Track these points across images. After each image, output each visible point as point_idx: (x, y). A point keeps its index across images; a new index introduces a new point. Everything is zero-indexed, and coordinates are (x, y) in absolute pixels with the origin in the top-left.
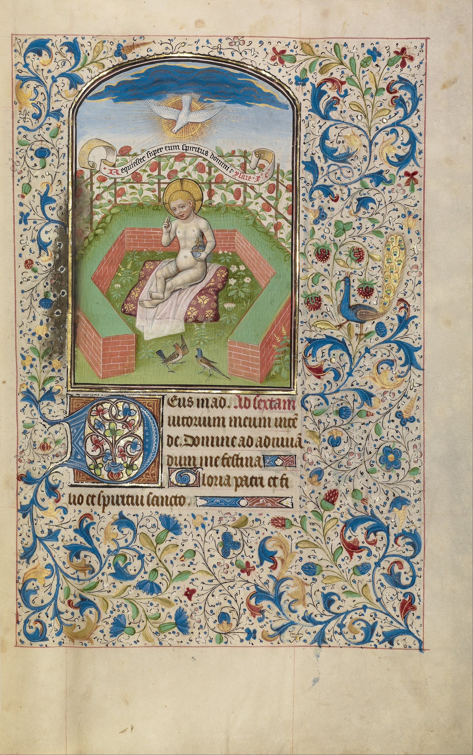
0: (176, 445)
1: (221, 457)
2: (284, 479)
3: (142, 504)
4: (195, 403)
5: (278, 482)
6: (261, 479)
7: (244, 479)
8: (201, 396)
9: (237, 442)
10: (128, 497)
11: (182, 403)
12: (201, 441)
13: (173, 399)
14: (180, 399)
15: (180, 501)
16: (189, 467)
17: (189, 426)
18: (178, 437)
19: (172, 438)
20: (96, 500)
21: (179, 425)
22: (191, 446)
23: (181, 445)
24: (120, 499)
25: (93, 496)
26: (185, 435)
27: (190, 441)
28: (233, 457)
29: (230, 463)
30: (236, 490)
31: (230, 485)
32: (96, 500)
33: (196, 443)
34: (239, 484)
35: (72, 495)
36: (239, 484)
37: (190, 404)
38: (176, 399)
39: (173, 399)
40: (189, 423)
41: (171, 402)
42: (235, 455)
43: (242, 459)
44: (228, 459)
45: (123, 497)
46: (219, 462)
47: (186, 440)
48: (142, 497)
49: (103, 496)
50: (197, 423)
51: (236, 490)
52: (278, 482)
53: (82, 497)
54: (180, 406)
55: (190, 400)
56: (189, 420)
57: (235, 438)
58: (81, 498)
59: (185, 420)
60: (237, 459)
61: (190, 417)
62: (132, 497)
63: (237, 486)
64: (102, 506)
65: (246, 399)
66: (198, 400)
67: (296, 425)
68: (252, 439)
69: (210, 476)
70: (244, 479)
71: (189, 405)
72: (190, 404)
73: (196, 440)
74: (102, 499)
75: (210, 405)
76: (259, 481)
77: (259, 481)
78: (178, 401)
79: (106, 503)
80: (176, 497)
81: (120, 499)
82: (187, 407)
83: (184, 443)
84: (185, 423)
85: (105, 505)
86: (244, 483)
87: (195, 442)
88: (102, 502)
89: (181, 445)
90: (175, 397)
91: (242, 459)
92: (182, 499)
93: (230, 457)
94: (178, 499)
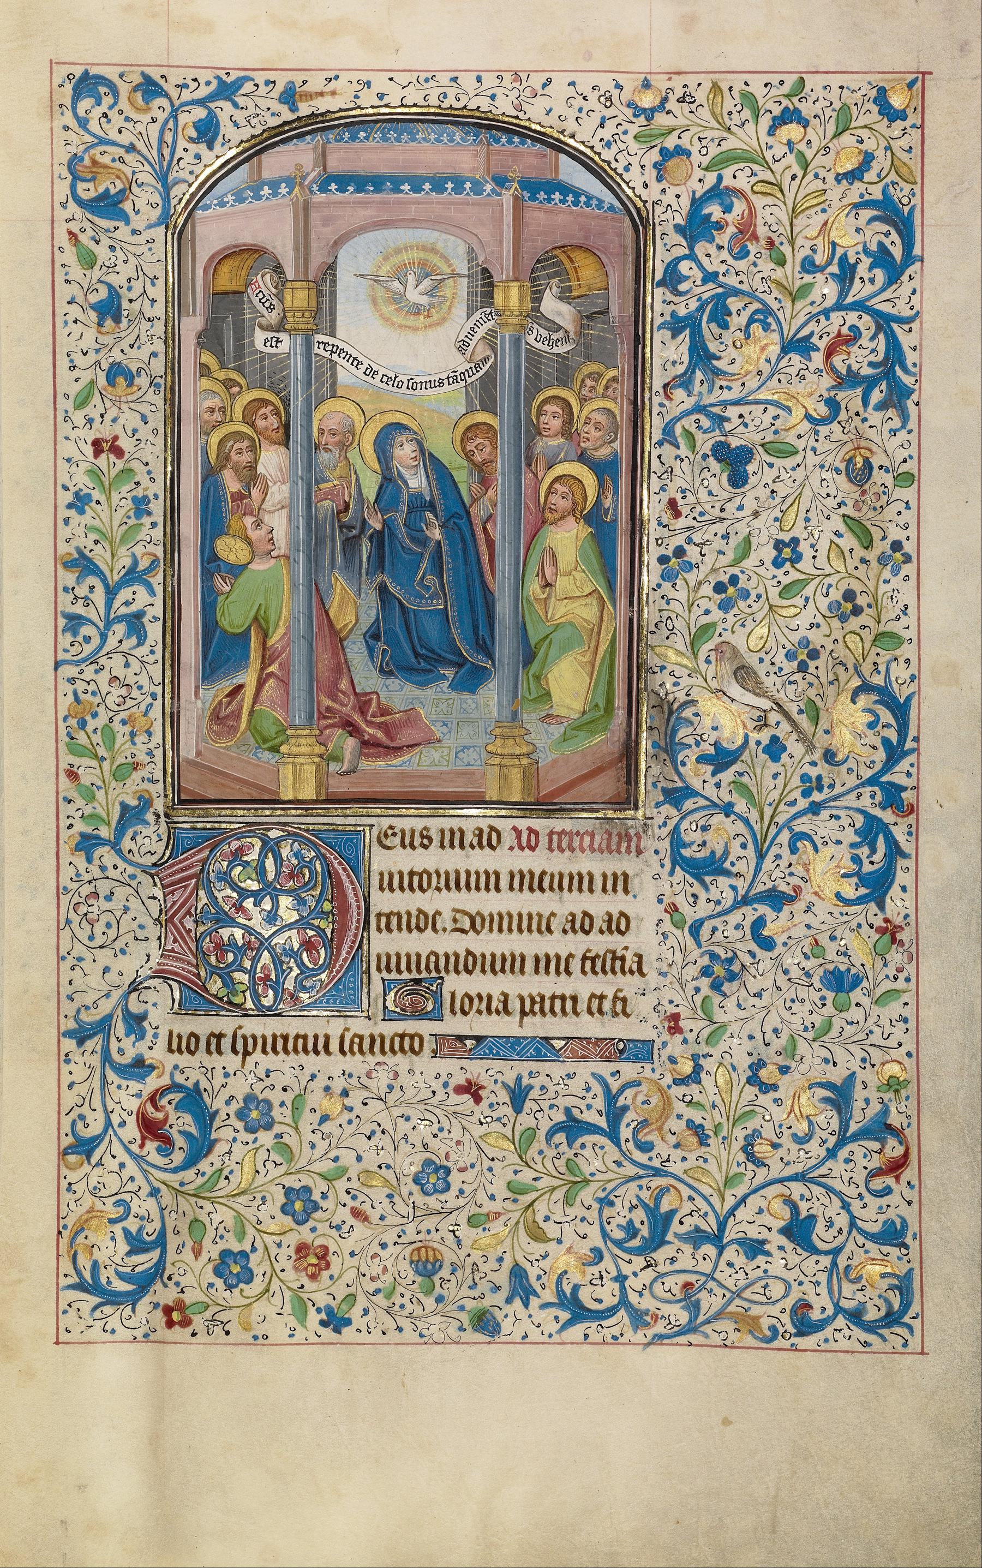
0: (435, 929)
3: (327, 1052)
4: (544, 840)
5: (607, 1005)
6: (575, 999)
7: (538, 999)
8: (447, 824)
12: (414, 921)
13: (390, 832)
14: (403, 832)
16: (398, 977)
18: (438, 913)
22: (463, 931)
23: (444, 930)
25: (220, 1037)
26: (456, 911)
28: (605, 955)
31: (507, 1011)
32: (226, 1043)
34: (527, 1009)
36: (527, 1009)
37: (426, 842)
38: (394, 834)
39: (390, 832)
41: (383, 838)
42: (608, 951)
44: (593, 960)
45: (285, 1038)
46: (575, 965)
47: (455, 920)
48: (327, 1037)
49: (245, 1038)
53: (197, 1038)
54: (403, 845)
55: (425, 833)
56: (425, 877)
58: (193, 1040)
59: (416, 879)
60: (614, 958)
61: (425, 871)
62: (305, 1037)
63: (523, 1013)
64: (240, 1055)
65: (530, 830)
66: (442, 832)
68: (591, 918)
69: (467, 995)
70: (538, 999)
72: (426, 842)
75: (467, 843)
76: (569, 1004)
77: (569, 1004)
78: (400, 834)
79: (250, 1049)
80: (402, 1036)
84: (415, 884)
85: (246, 1053)
86: (537, 1008)
87: (476, 923)
88: (240, 1046)
90: (391, 827)
92: (417, 1040)
93: (597, 956)
94: (407, 1040)
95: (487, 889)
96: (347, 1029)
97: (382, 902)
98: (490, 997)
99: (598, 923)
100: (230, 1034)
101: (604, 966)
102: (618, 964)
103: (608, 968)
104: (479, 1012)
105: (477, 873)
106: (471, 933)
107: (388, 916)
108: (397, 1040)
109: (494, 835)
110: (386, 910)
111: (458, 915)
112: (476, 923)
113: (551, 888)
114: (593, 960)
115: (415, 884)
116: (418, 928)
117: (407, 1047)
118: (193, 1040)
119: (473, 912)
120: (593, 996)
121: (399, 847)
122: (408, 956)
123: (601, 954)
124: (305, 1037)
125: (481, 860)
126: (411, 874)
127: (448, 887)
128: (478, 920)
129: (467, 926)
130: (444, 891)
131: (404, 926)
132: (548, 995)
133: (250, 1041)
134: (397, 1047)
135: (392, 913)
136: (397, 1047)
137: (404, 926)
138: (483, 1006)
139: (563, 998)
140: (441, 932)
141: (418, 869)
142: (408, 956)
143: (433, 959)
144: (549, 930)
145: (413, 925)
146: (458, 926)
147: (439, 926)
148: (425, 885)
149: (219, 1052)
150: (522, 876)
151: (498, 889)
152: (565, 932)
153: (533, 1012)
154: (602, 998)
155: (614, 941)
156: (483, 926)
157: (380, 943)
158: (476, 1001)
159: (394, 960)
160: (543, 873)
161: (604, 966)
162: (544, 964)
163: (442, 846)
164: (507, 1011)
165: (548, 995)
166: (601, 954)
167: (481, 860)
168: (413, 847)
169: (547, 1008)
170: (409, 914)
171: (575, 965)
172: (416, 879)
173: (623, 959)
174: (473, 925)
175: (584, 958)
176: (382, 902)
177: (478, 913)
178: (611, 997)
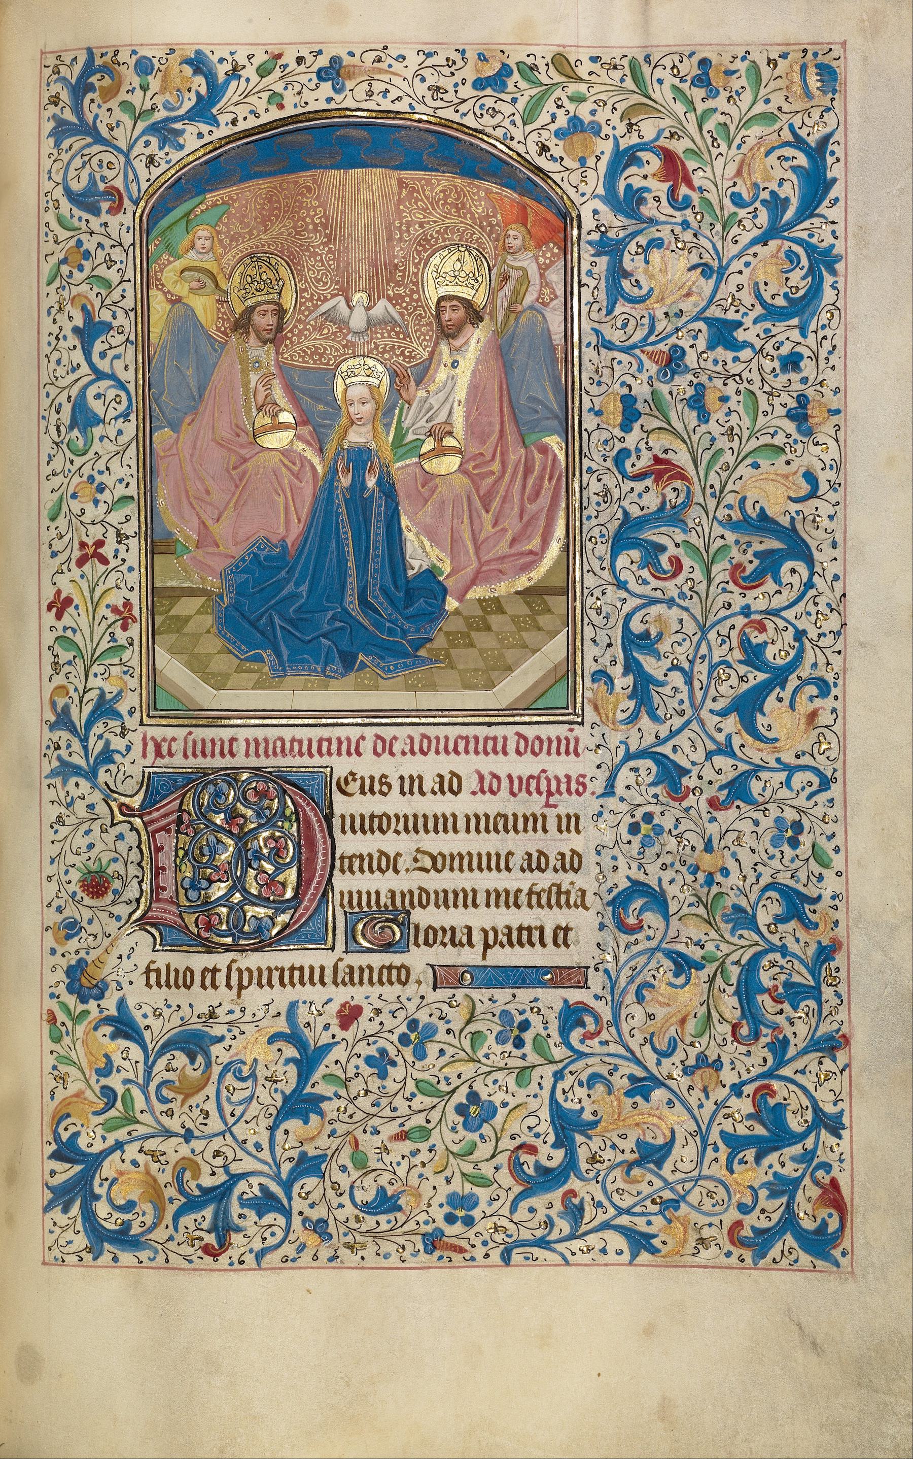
0: (396, 871)
1: (526, 891)
6: (542, 929)
9: (515, 862)
10: (292, 969)
17: (383, 832)
18: (399, 855)
19: (388, 858)
20: (221, 978)
22: (427, 871)
25: (215, 970)
27: (428, 863)
28: (550, 888)
30: (484, 957)
32: (221, 978)
33: (439, 866)
34: (491, 942)
35: (172, 969)
37: (385, 789)
41: (343, 786)
42: (553, 885)
47: (416, 860)
50: (401, 827)
51: (484, 957)
53: (192, 973)
54: (363, 792)
58: (188, 974)
59: (376, 821)
60: (559, 893)
61: (385, 814)
63: (487, 946)
64: (235, 989)
72: (385, 789)
74: (234, 976)
76: (536, 935)
77: (536, 935)
79: (245, 983)
80: (390, 968)
84: (376, 825)
85: (241, 987)
87: (438, 862)
88: (234, 981)
92: (403, 972)
93: (543, 890)
95: (446, 830)
97: (348, 844)
98: (453, 929)
99: (552, 862)
101: (549, 900)
102: (563, 898)
103: (553, 901)
104: (444, 944)
106: (432, 872)
108: (385, 971)
109: (455, 780)
110: (349, 853)
112: (438, 862)
113: (525, 830)
114: (539, 895)
115: (376, 825)
116: (380, 868)
118: (188, 974)
120: (558, 927)
122: (369, 894)
124: (301, 969)
125: (444, 805)
126: (372, 816)
127: (407, 830)
128: (440, 860)
130: (403, 833)
132: (515, 926)
133: (246, 975)
134: (385, 979)
135: (354, 856)
136: (385, 979)
139: (529, 929)
142: (369, 894)
143: (279, 744)
144: (508, 869)
146: (419, 865)
147: (400, 866)
149: (214, 986)
150: (445, 818)
151: (455, 831)
152: (523, 870)
155: (566, 879)
156: (444, 866)
157: (341, 882)
158: (440, 934)
161: (549, 900)
162: (508, 899)
163: (403, 793)
164: (470, 943)
165: (515, 926)
167: (444, 805)
168: (372, 792)
171: (481, 899)
172: (376, 821)
173: (568, 893)
175: (530, 893)
176: (348, 844)
177: (440, 854)
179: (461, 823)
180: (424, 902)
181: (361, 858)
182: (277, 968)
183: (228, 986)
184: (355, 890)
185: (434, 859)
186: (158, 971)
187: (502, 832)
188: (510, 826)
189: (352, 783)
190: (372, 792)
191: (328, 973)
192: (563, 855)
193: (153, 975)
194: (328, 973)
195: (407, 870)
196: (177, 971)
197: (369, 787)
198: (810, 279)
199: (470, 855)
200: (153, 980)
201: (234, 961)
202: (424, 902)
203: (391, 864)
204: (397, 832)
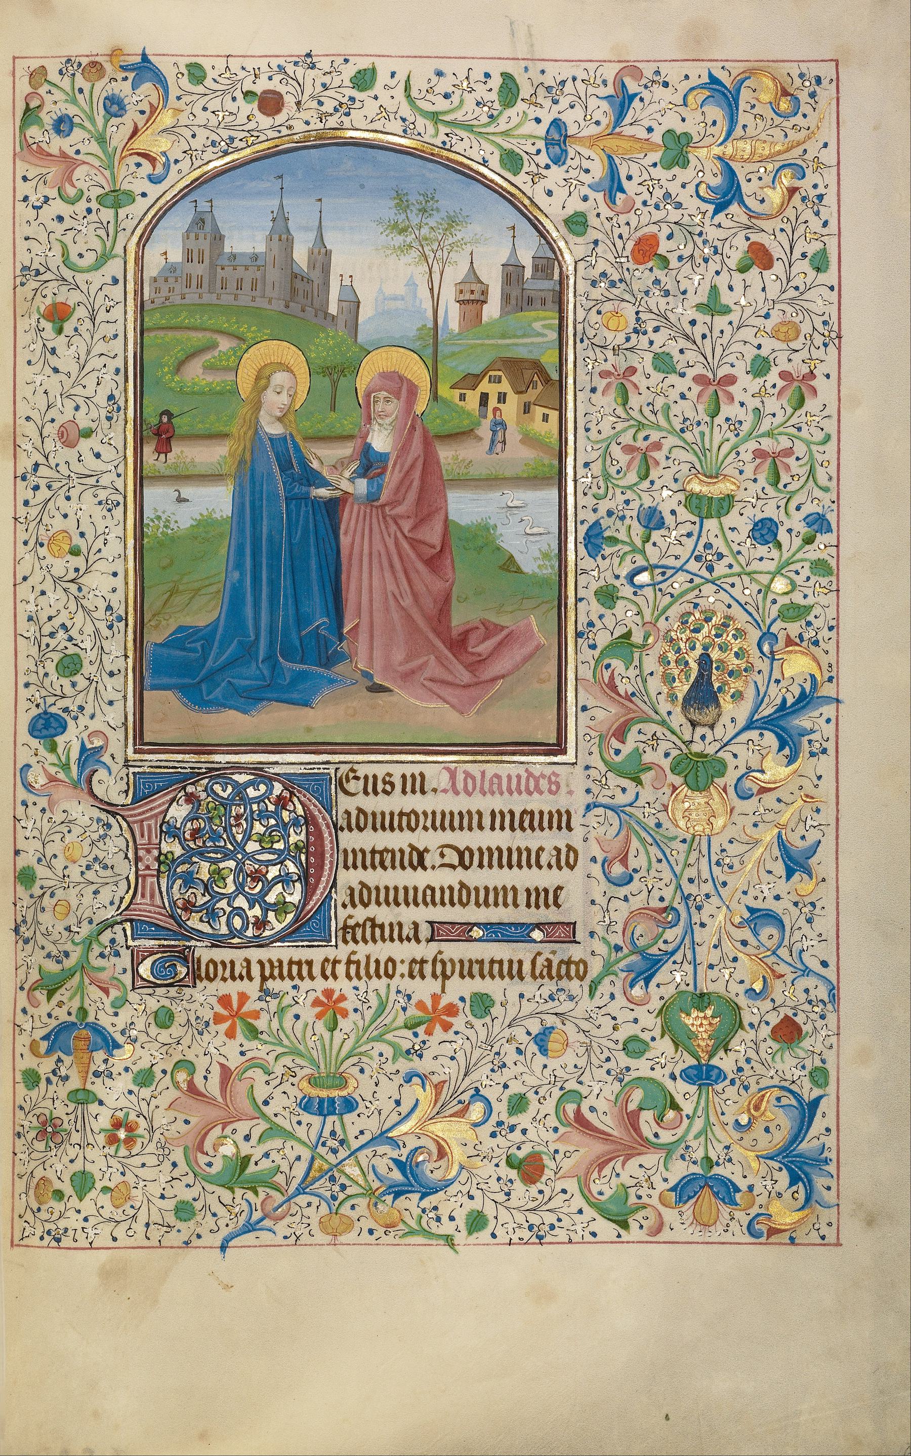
0: (425, 868)
2: (354, 962)
5: (341, 969)
6: (310, 963)
7: (276, 964)
8: (408, 770)
11: (372, 787)
15: (577, 971)
17: (413, 830)
20: (428, 968)
21: (392, 829)
22: (453, 867)
24: (476, 968)
27: (454, 859)
29: (359, 936)
31: (250, 979)
32: (428, 968)
34: (267, 973)
35: (372, 960)
36: (267, 973)
37: (388, 788)
38: (357, 778)
39: (351, 775)
40: (413, 824)
42: (369, 919)
43: (382, 927)
44: (353, 928)
45: (481, 962)
47: (442, 855)
52: (341, 969)
55: (553, 779)
56: (413, 817)
57: (541, 849)
58: (390, 964)
59: (405, 819)
60: (374, 926)
62: (501, 962)
63: (264, 979)
64: (440, 979)
65: (467, 774)
66: (404, 777)
67: (573, 825)
70: (276, 964)
71: (385, 792)
72: (388, 788)
73: (467, 854)
76: (305, 968)
77: (305, 968)
78: (362, 782)
79: (449, 973)
80: (568, 963)
81: (476, 968)
82: (381, 795)
83: (438, 861)
84: (404, 824)
85: (445, 977)
86: (276, 972)
89: (433, 867)
91: (382, 927)
92: (582, 967)
93: (357, 925)
94: (573, 967)
96: (539, 954)
98: (232, 963)
100: (430, 960)
102: (378, 931)
105: (452, 814)
107: (381, 853)
111: (447, 851)
115: (404, 824)
117: (573, 973)
119: (462, 849)
121: (361, 794)
123: (361, 922)
124: (501, 962)
126: (401, 814)
129: (456, 861)
131: (397, 863)
135: (386, 850)
137: (397, 863)
138: (227, 974)
139: (299, 963)
140: (429, 870)
141: (407, 810)
144: (540, 867)
145: (406, 863)
146: (446, 860)
148: (413, 824)
153: (272, 976)
154: (423, 962)
159: (411, 893)
160: (524, 812)
163: (404, 792)
164: (250, 979)
166: (361, 922)
168: (376, 793)
169: (285, 973)
170: (402, 851)
171: (522, 898)
172: (405, 819)
174: (462, 863)
177: (468, 848)
178: (344, 960)
179: (487, 822)
180: (464, 900)
181: (393, 852)
182: (477, 962)
183: (434, 976)
184: (391, 886)
185: (461, 854)
186: (358, 963)
187: (537, 830)
188: (536, 824)
189: (353, 782)
190: (376, 793)
191: (527, 967)
192: (558, 851)
193: (353, 968)
194: (527, 967)
195: (433, 867)
196: (377, 962)
197: (372, 787)
198: (110, 150)
199: (499, 850)
200: (353, 971)
201: (440, 952)
202: (464, 900)
203: (419, 860)
204: (425, 828)
